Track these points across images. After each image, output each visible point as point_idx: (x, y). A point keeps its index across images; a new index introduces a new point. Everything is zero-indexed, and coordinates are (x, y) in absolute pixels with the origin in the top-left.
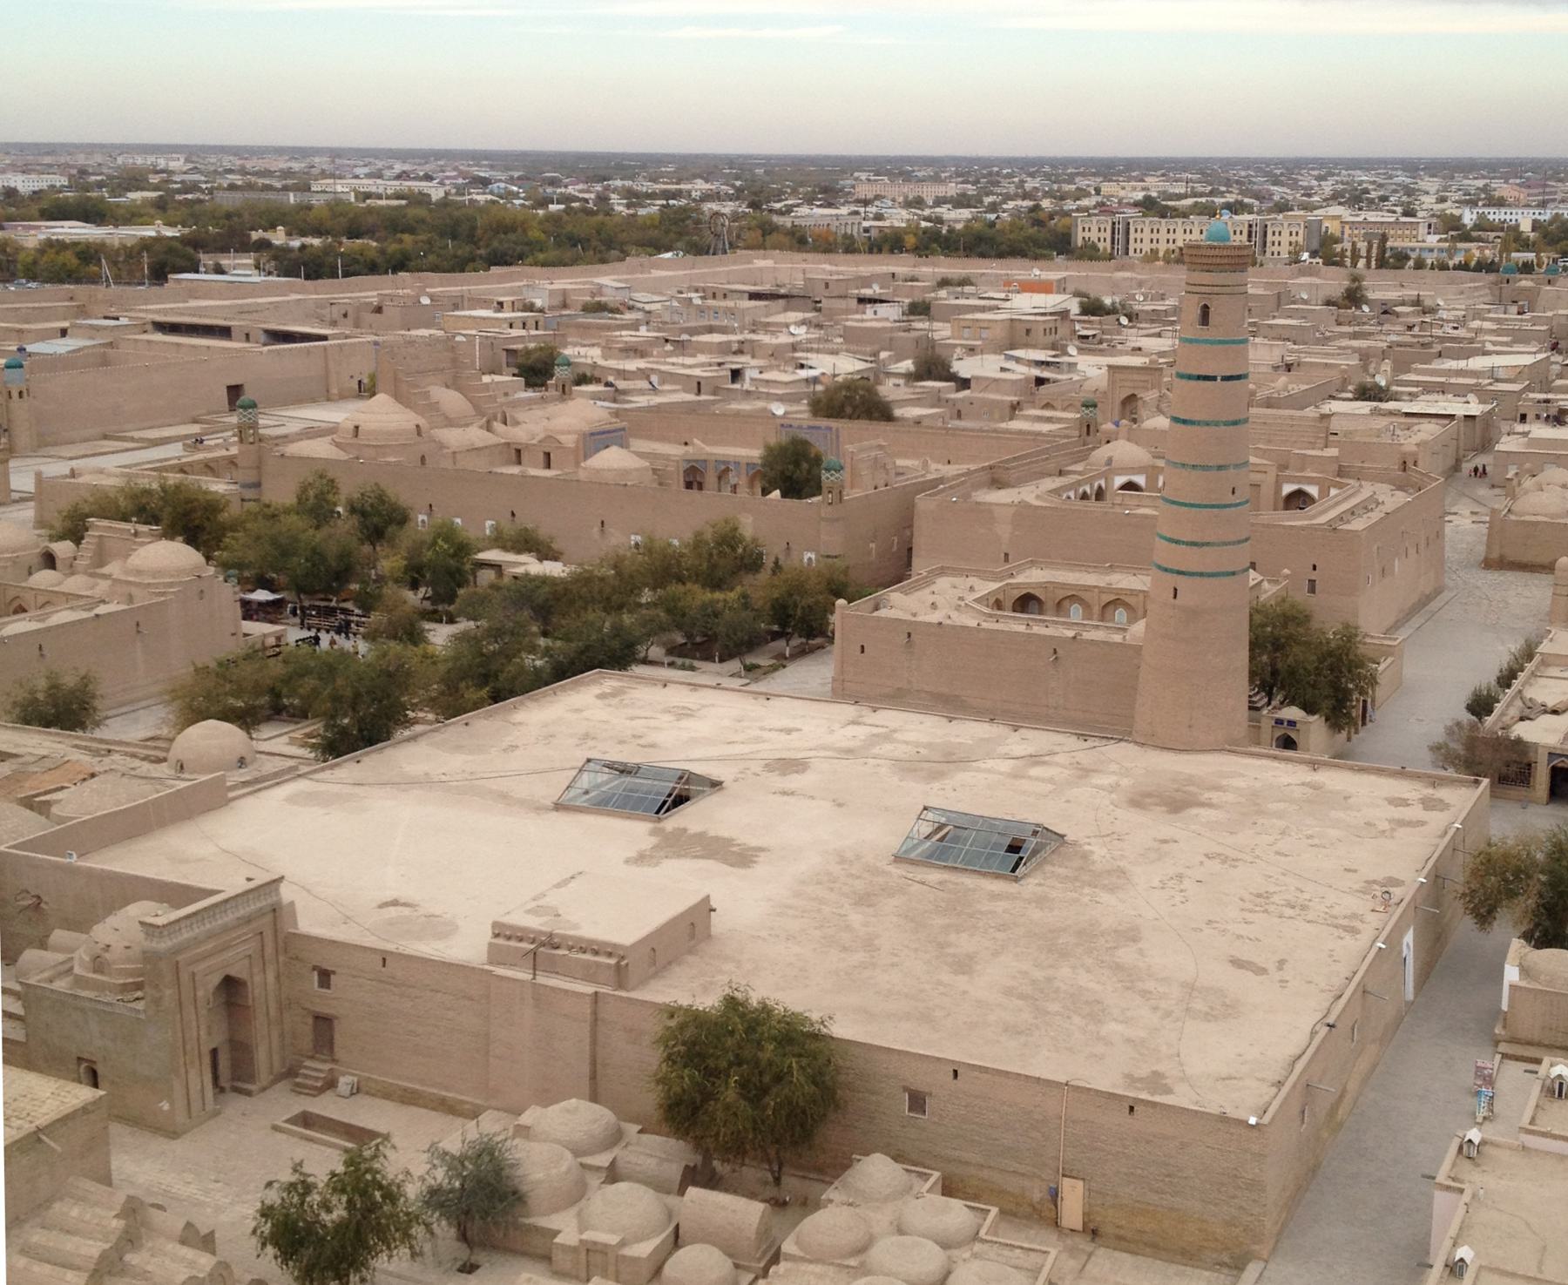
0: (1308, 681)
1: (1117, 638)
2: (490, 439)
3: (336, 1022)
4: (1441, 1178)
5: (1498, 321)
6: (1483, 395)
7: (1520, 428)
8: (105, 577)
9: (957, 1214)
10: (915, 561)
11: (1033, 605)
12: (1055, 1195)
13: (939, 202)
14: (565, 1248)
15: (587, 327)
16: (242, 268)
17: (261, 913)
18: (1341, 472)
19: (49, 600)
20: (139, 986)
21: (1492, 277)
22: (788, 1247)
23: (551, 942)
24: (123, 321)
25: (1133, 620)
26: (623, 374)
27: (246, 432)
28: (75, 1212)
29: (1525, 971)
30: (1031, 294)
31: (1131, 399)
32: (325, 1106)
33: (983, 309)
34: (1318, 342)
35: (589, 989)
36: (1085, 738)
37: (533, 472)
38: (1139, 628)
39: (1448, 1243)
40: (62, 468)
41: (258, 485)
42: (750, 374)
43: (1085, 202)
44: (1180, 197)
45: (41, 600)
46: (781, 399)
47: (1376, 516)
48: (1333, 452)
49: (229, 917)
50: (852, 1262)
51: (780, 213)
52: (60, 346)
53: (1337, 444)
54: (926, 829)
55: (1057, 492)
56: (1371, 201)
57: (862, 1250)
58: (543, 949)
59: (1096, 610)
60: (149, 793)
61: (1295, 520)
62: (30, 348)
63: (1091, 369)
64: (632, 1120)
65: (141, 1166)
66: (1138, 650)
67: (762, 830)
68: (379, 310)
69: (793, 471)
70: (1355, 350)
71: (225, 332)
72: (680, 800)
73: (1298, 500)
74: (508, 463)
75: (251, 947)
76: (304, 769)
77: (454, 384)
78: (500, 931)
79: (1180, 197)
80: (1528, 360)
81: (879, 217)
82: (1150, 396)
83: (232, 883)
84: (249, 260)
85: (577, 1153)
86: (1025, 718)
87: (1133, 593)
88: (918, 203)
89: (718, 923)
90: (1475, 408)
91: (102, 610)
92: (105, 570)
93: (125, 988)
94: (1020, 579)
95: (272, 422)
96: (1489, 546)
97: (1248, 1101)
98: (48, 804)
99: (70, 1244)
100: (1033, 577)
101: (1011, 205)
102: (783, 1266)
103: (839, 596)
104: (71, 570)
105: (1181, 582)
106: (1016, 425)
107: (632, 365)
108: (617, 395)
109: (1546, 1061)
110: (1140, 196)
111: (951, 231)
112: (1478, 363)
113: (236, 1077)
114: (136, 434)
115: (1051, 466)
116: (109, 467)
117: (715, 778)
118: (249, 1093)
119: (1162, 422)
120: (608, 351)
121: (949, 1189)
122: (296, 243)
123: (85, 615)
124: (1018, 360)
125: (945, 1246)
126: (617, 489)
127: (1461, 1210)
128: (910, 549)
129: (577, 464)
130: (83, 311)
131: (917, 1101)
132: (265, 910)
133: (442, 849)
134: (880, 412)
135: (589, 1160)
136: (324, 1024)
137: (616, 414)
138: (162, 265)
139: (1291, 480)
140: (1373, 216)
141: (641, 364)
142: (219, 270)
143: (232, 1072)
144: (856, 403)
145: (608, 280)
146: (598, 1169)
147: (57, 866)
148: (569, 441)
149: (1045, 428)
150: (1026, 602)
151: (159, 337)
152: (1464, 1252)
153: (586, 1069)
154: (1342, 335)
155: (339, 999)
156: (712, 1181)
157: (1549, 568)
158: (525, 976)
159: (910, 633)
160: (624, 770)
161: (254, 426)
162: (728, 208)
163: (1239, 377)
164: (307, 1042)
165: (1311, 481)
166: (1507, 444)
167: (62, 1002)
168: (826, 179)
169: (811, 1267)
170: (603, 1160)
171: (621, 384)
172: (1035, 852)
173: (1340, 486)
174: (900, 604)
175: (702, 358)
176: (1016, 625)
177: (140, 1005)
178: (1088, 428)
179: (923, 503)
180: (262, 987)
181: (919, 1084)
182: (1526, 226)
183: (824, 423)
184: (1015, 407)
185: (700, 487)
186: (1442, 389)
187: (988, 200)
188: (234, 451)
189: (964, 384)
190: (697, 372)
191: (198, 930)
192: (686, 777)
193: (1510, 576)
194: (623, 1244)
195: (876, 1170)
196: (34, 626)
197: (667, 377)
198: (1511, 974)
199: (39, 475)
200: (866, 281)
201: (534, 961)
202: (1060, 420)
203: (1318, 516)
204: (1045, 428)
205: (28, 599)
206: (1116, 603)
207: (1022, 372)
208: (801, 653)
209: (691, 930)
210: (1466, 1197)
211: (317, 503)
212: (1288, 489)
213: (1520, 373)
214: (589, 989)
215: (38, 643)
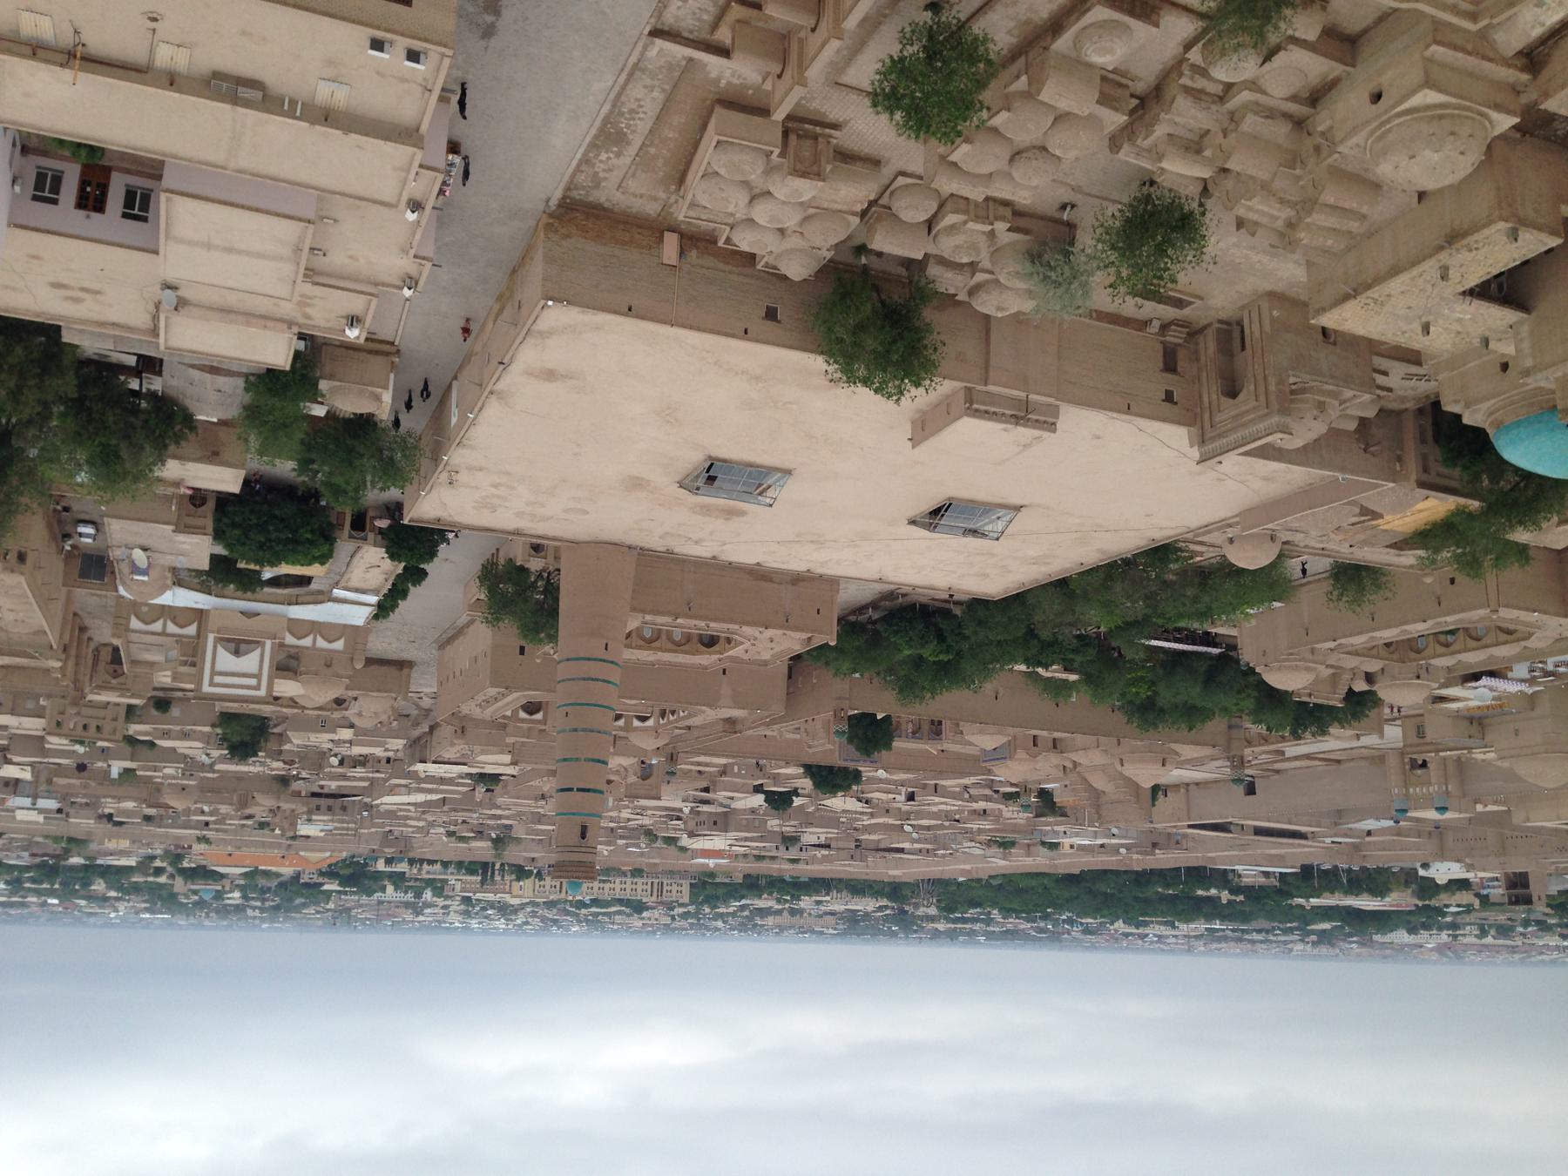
0: (523, 591)
1: (648, 618)
2: (1075, 757)
3: (1161, 365)
4: (428, 265)
5: (407, 826)
6: (414, 776)
7: (390, 754)
8: (1332, 666)
9: (745, 241)
10: (785, 670)
11: (706, 641)
12: (682, 253)
13: (779, 912)
14: (1003, 219)
15: (1013, 831)
16: (1250, 873)
17: (1213, 439)
18: (504, 726)
19: (1368, 652)
20: (1293, 392)
21: (411, 855)
22: (857, 220)
23: (1017, 420)
24: (1328, 840)
25: (639, 630)
26: (987, 799)
27: (1240, 763)
28: (1330, 242)
29: (378, 398)
30: (715, 849)
31: (645, 777)
32: (1169, 312)
33: (746, 839)
34: (524, 813)
35: (991, 388)
36: (668, 552)
37: (1045, 733)
38: (633, 624)
39: (423, 223)
40: (1365, 741)
41: (1230, 727)
42: (902, 798)
43: (681, 910)
44: (619, 913)
45: (1374, 652)
46: (880, 781)
47: (480, 698)
48: (510, 740)
49: (1232, 438)
50: (812, 211)
51: (886, 907)
52: (1370, 824)
53: (507, 745)
54: (770, 493)
55: (690, 716)
56: (492, 907)
57: (807, 219)
58: (1022, 414)
59: (664, 637)
60: (1292, 520)
61: (535, 695)
62: (1391, 823)
63: (672, 798)
64: (960, 303)
65: (1289, 272)
66: (633, 609)
67: (869, 490)
68: (1154, 845)
69: (870, 733)
70: (499, 807)
71: (1259, 831)
72: (936, 512)
73: (532, 708)
74: (1061, 740)
75: (1218, 418)
76: (1190, 536)
77: (1097, 794)
78: (1051, 427)
79: (619, 913)
80: (387, 799)
81: (818, 903)
82: (632, 779)
83: (1233, 463)
84: (1245, 880)
85: (997, 282)
86: (707, 564)
87: (640, 647)
88: (793, 912)
89: (906, 430)
90: (420, 767)
91: (1332, 645)
92: (1331, 671)
93: (1303, 391)
94: (715, 657)
95: (1217, 769)
96: (409, 676)
97: (556, 316)
98: (1361, 514)
99: (1332, 221)
100: (707, 659)
101: (731, 910)
102: (859, 208)
103: (836, 647)
104: (1354, 672)
105: (601, 654)
106: (723, 761)
107: (982, 805)
108: (991, 784)
109: (362, 341)
110: (645, 914)
111: (770, 894)
112: (420, 798)
113: (1229, 333)
114: (1317, 763)
115: (696, 733)
116: (1337, 741)
117: (913, 528)
118: (1220, 321)
119: (615, 762)
120: (998, 816)
121: (751, 258)
122: (1213, 892)
123: (1343, 641)
124: (722, 805)
125: (751, 221)
126: (985, 720)
127: (415, 243)
128: (790, 677)
129: (1015, 737)
130: (1356, 847)
131: (771, 314)
132: (1210, 443)
133: (1101, 482)
134: (812, 771)
135: (987, 276)
136: (1170, 366)
137: (989, 772)
138: (1310, 877)
139: (538, 722)
140: (490, 897)
141: (975, 806)
142: (1267, 874)
143: (1231, 334)
144: (830, 778)
145: (999, 863)
146: (984, 271)
147: (1352, 473)
148: (1021, 754)
149: (702, 759)
150: (710, 642)
151: (1303, 829)
152: (411, 217)
153: (994, 337)
154: (508, 818)
155: (1160, 382)
156: (908, 263)
157: (370, 661)
158: (1032, 397)
159: (786, 623)
160: (974, 532)
161: (1233, 767)
162: (921, 911)
163: (563, 790)
164: (1182, 355)
165: (523, 721)
166: (398, 744)
167: (1348, 381)
168: (854, 925)
169: (839, 207)
170: (980, 277)
171: (988, 792)
172: (697, 477)
173: (504, 717)
174: (794, 642)
175: (935, 809)
176: (716, 627)
177: (1292, 380)
178: (672, 758)
179: (779, 709)
180: (1211, 391)
181: (770, 324)
182: (390, 889)
183: (851, 765)
184: (723, 773)
185: (932, 722)
186: (442, 781)
187: (746, 913)
188: (1248, 751)
189: (758, 789)
190: (937, 799)
191: (1253, 429)
192: (932, 527)
193: (394, 657)
194: (965, 223)
195: (797, 270)
196: (1377, 634)
197: (954, 796)
198: (387, 397)
199: (1382, 736)
200: (825, 859)
201: (1026, 406)
202: (692, 764)
203: (517, 698)
204: (702, 759)
205: (1383, 653)
206: (650, 641)
207: (721, 795)
208: (861, 609)
209: (924, 428)
210: (412, 252)
211: (1191, 715)
212: (539, 716)
213: (392, 791)
214: (991, 388)
215: (1374, 622)
